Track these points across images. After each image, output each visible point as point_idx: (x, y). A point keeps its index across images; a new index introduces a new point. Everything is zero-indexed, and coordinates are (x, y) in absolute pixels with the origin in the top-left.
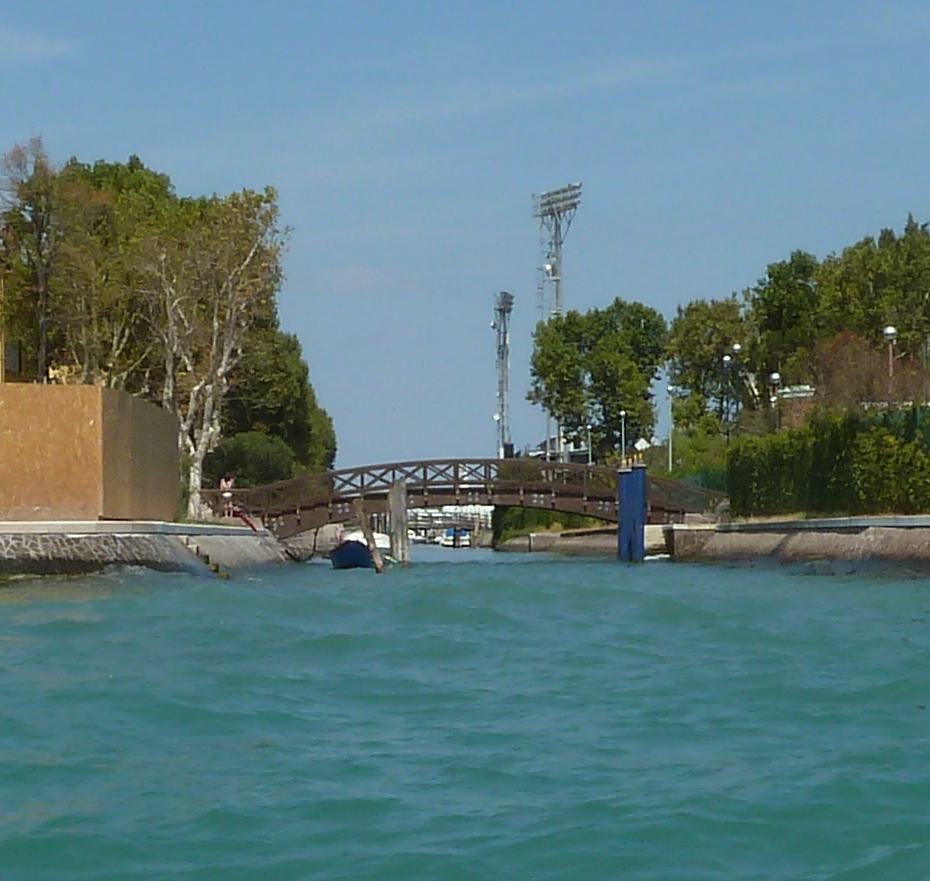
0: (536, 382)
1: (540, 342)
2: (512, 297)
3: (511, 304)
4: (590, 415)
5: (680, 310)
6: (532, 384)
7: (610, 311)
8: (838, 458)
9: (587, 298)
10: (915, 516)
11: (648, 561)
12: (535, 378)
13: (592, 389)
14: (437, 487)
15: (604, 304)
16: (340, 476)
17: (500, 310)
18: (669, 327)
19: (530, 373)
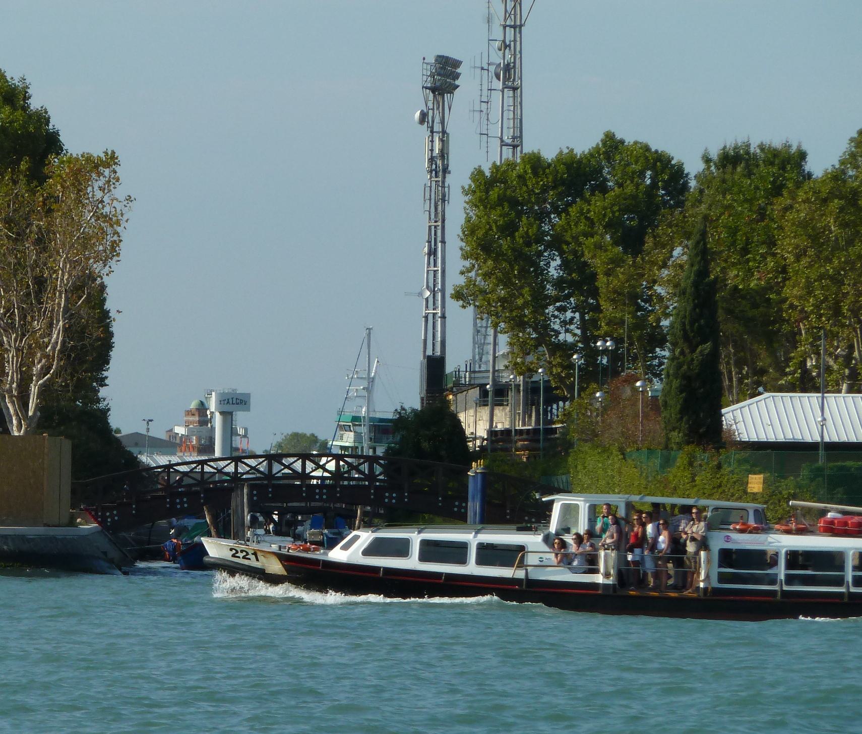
0: (469, 270)
1: (604, 142)
2: (457, 64)
3: (457, 76)
4: (556, 327)
5: (707, 160)
6: (462, 273)
7: (594, 153)
8: (456, 509)
9: (560, 130)
10: (437, 600)
11: (782, 456)
12: (467, 264)
13: (559, 283)
14: (338, 571)
15: (584, 142)
16: (246, 461)
17: (433, 90)
18: (693, 184)
19: (459, 253)
